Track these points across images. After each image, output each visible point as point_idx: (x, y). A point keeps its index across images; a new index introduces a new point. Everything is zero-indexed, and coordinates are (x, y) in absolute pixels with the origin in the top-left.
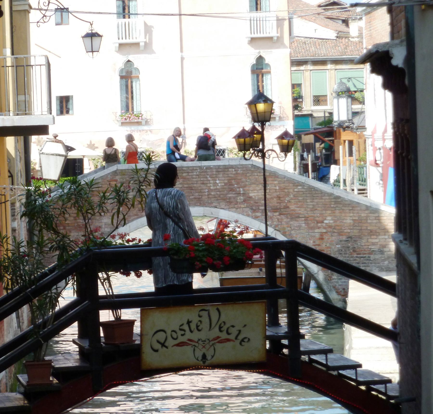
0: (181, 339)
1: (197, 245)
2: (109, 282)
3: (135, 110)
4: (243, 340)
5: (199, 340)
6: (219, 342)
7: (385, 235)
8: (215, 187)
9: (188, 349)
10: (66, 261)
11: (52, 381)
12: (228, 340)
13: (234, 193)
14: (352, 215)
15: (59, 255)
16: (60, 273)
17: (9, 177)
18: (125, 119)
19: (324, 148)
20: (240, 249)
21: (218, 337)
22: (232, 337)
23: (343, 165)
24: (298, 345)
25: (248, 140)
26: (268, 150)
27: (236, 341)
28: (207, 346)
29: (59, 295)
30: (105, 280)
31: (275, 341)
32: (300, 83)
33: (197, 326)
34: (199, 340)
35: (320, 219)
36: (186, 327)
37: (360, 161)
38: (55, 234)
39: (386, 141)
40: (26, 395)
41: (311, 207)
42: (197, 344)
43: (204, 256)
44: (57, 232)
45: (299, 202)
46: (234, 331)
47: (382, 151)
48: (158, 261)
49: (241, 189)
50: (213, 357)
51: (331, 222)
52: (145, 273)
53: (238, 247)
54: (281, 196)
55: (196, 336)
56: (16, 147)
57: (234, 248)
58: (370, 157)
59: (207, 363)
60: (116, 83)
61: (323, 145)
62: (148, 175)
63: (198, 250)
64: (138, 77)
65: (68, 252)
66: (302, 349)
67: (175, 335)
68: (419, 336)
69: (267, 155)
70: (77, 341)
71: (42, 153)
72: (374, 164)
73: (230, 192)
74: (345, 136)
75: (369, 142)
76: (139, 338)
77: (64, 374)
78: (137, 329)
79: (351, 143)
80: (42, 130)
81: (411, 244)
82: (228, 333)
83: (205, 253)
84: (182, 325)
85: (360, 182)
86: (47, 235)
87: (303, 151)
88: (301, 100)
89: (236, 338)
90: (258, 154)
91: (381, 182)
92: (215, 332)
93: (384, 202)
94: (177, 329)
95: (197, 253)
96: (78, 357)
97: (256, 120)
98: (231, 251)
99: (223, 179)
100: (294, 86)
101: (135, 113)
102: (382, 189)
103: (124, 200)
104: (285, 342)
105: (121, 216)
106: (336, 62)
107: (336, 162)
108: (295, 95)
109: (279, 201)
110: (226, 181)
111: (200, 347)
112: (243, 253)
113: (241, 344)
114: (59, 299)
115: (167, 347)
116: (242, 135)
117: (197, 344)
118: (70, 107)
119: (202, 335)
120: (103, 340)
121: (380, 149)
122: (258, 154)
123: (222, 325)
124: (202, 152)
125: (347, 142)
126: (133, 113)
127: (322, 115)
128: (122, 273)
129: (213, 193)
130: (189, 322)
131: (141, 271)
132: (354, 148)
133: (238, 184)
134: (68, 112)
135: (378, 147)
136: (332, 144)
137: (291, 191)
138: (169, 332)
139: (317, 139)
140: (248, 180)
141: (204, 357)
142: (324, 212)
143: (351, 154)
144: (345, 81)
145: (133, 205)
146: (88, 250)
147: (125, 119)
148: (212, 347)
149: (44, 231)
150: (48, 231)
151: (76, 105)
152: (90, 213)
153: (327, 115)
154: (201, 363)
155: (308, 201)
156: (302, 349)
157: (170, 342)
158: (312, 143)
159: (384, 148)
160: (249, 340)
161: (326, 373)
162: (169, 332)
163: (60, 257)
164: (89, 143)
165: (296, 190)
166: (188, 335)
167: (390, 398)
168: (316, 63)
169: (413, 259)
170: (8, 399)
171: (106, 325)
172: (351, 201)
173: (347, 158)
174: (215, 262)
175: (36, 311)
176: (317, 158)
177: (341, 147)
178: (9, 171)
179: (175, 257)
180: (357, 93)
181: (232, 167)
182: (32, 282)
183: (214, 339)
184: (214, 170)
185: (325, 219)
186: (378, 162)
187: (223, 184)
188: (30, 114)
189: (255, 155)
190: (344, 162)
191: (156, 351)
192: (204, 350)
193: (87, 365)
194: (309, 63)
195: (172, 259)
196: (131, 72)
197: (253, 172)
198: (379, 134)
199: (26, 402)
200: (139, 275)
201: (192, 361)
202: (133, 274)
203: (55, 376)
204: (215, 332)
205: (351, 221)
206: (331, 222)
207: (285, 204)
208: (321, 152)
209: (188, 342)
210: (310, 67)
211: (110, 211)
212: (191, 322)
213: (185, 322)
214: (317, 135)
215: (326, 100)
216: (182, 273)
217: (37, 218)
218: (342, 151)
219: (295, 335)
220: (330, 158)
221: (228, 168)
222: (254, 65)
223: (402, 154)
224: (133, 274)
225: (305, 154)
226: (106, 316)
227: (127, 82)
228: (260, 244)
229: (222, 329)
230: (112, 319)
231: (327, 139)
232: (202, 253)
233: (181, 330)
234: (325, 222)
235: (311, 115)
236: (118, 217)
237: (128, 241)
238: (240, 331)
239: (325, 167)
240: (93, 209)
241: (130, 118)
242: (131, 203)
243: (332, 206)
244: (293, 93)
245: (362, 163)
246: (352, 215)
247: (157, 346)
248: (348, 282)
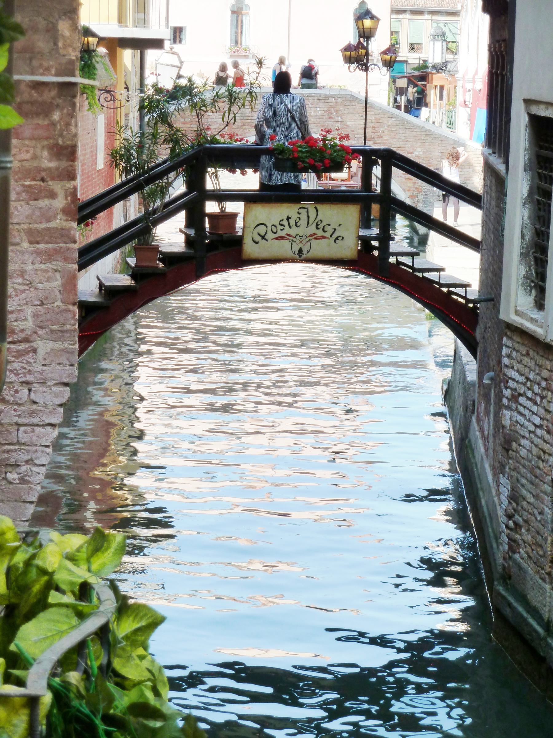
0: (280, 233)
1: (300, 147)
2: (217, 177)
3: (243, 44)
4: (337, 238)
5: (297, 235)
6: (315, 239)
7: (470, 168)
8: (315, 114)
9: (286, 244)
10: (178, 154)
11: (158, 264)
12: (323, 237)
13: (332, 120)
14: (440, 148)
15: (171, 148)
16: (171, 164)
17: (125, 88)
18: (234, 52)
19: (416, 91)
20: (340, 153)
21: (315, 234)
22: (327, 235)
23: (433, 108)
24: (388, 247)
25: (353, 53)
26: (372, 65)
27: (331, 238)
28: (304, 242)
29: (170, 184)
30: (213, 174)
31: (366, 241)
32: (397, 30)
33: (296, 223)
34: (297, 235)
35: (411, 150)
36: (285, 223)
37: (450, 105)
38: (169, 128)
39: (476, 83)
40: (134, 276)
41: (403, 138)
42: (294, 239)
43: (306, 157)
44: (170, 126)
45: (393, 132)
46: (329, 230)
47: (471, 93)
48: (265, 159)
49: (340, 118)
50: (308, 252)
51: (421, 153)
52: (250, 171)
53: (339, 150)
54: (376, 126)
55: (294, 231)
56: (132, 61)
57: (335, 152)
58: (460, 98)
59: (303, 257)
60: (228, 16)
61: (416, 89)
62: (259, 78)
63: (301, 151)
64: (248, 13)
65: (180, 146)
66: (391, 250)
67: (274, 229)
68: (503, 235)
69: (370, 69)
70: (184, 230)
71: (159, 63)
72: (463, 104)
73: (329, 120)
74: (437, 80)
75: (460, 84)
76: (242, 231)
77: (170, 259)
78: (239, 223)
79: (442, 88)
80: (157, 44)
81: (500, 156)
82: (324, 231)
83: (308, 155)
84: (283, 220)
85: (448, 125)
86: (162, 128)
87: (397, 95)
88: (398, 46)
89: (331, 236)
90: (362, 67)
91: (469, 122)
92: (312, 229)
93: (471, 138)
94: (277, 224)
95: (300, 154)
96: (184, 245)
97: (363, 35)
98: (331, 155)
99: (324, 106)
100: (392, 33)
101: (243, 47)
102: (469, 128)
103: (235, 99)
104: (375, 243)
105: (232, 115)
106: (433, 13)
107: (427, 105)
108: (393, 41)
109: (374, 131)
110: (326, 109)
111: (298, 242)
112: (342, 157)
113: (335, 241)
114: (170, 189)
115: (267, 240)
116: (348, 48)
117: (294, 239)
118: (183, 36)
119: (300, 231)
120: (208, 230)
121: (469, 91)
122: (362, 67)
123: (319, 223)
124: (305, 81)
125: (438, 87)
126: (242, 47)
127: (417, 61)
128: (228, 170)
129: (313, 120)
130: (288, 218)
131: (247, 169)
132: (445, 93)
133: (336, 112)
134: (180, 42)
135: (468, 89)
136: (424, 88)
137: (386, 122)
138: (269, 226)
139: (410, 82)
140: (347, 110)
141: (300, 251)
142: (415, 144)
143: (441, 98)
144: (441, 25)
145: (243, 105)
146: (200, 144)
147: (234, 52)
148: (309, 243)
149: (159, 124)
150: (162, 125)
151: (187, 35)
152: (204, 111)
153: (421, 62)
154: (298, 256)
155: (400, 132)
156: (391, 250)
157: (270, 236)
158: (406, 88)
159: (474, 90)
160: (343, 238)
161: (412, 274)
162: (269, 226)
163: (173, 150)
164: (199, 72)
165: (390, 121)
166: (287, 230)
167: (468, 301)
168: (414, 12)
169: (501, 168)
170: (117, 279)
171: (212, 217)
172: (440, 135)
173: (438, 102)
174: (316, 164)
175: (147, 198)
176: (408, 100)
177: (433, 91)
178: (125, 83)
179: (280, 157)
180: (451, 43)
181: (332, 96)
182: (145, 172)
183: (311, 236)
184: (316, 98)
185: (415, 150)
186: (467, 103)
187: (323, 112)
188: (148, 27)
189: (359, 68)
190: (435, 106)
191: (257, 243)
192: (301, 245)
193: (192, 251)
194: (408, 12)
195: (276, 159)
196: (242, 8)
197: (351, 102)
198: (470, 76)
199: (133, 282)
200: (243, 174)
201: (289, 254)
202: (238, 171)
203: (160, 260)
204: (312, 229)
205: (440, 154)
206: (421, 153)
207: (379, 134)
208: (414, 95)
209: (287, 236)
210: (408, 16)
211: (221, 109)
212: (290, 218)
213: (285, 218)
214: (411, 78)
215: (421, 49)
216: (286, 171)
217: (154, 112)
218: (432, 95)
219: (385, 237)
220: (421, 101)
221: (328, 97)
222: (357, 9)
223: (496, 72)
224: (238, 171)
225: (398, 98)
226: (211, 207)
227: (237, 17)
228: (358, 149)
229: (319, 227)
230: (218, 210)
231: (420, 83)
232: (305, 155)
233: (281, 225)
234: (415, 153)
235: (406, 62)
236: (229, 116)
237: (237, 140)
238: (335, 230)
239: (416, 109)
240: (206, 107)
241: (238, 51)
242: (242, 101)
243: (423, 138)
244: (391, 39)
245: (451, 107)
246: (440, 148)
247: (258, 238)
248: (433, 210)
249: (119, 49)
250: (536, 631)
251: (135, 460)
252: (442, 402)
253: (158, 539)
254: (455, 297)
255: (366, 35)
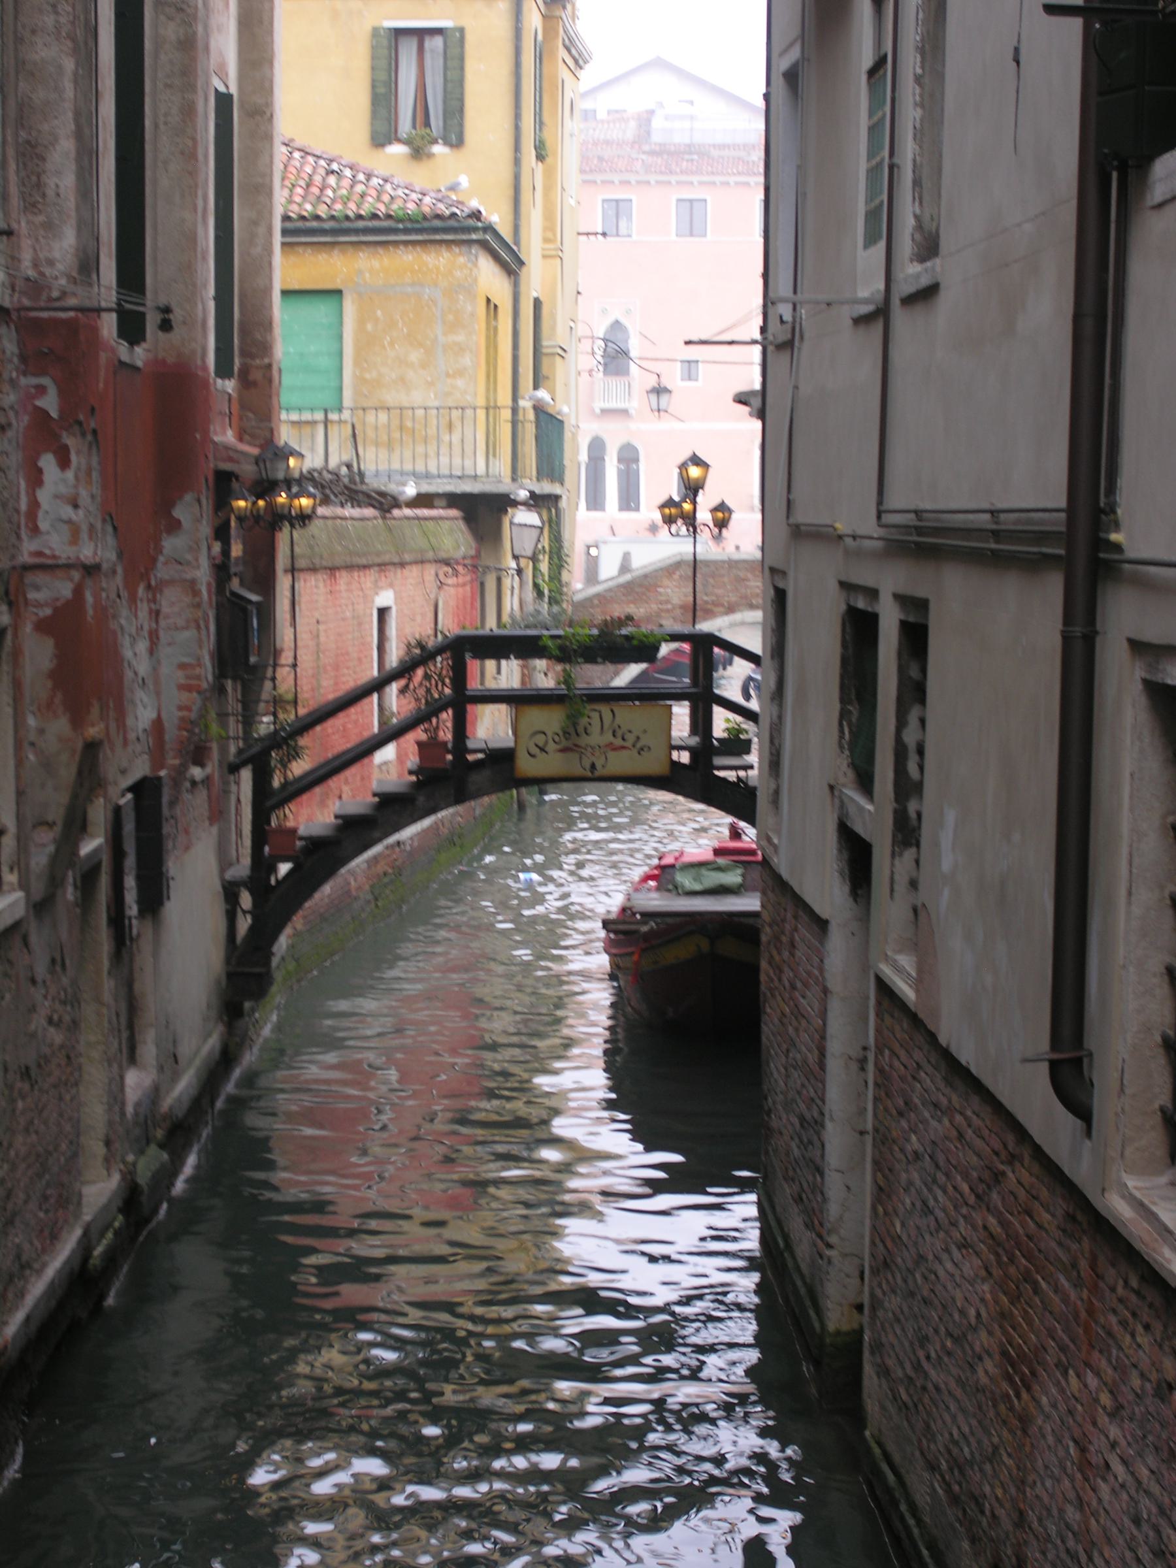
12: (623, 748)
46: (631, 739)
82: (623, 739)
89: (634, 746)
116: (670, 503)
138: (550, 734)
183: (607, 746)
204: (608, 737)
247: (536, 751)
249: (468, 693)
250: (425, 831)
251: (534, 1047)
252: (734, 516)
253: (514, 1094)
254: (736, 1190)
255: (692, 489)
